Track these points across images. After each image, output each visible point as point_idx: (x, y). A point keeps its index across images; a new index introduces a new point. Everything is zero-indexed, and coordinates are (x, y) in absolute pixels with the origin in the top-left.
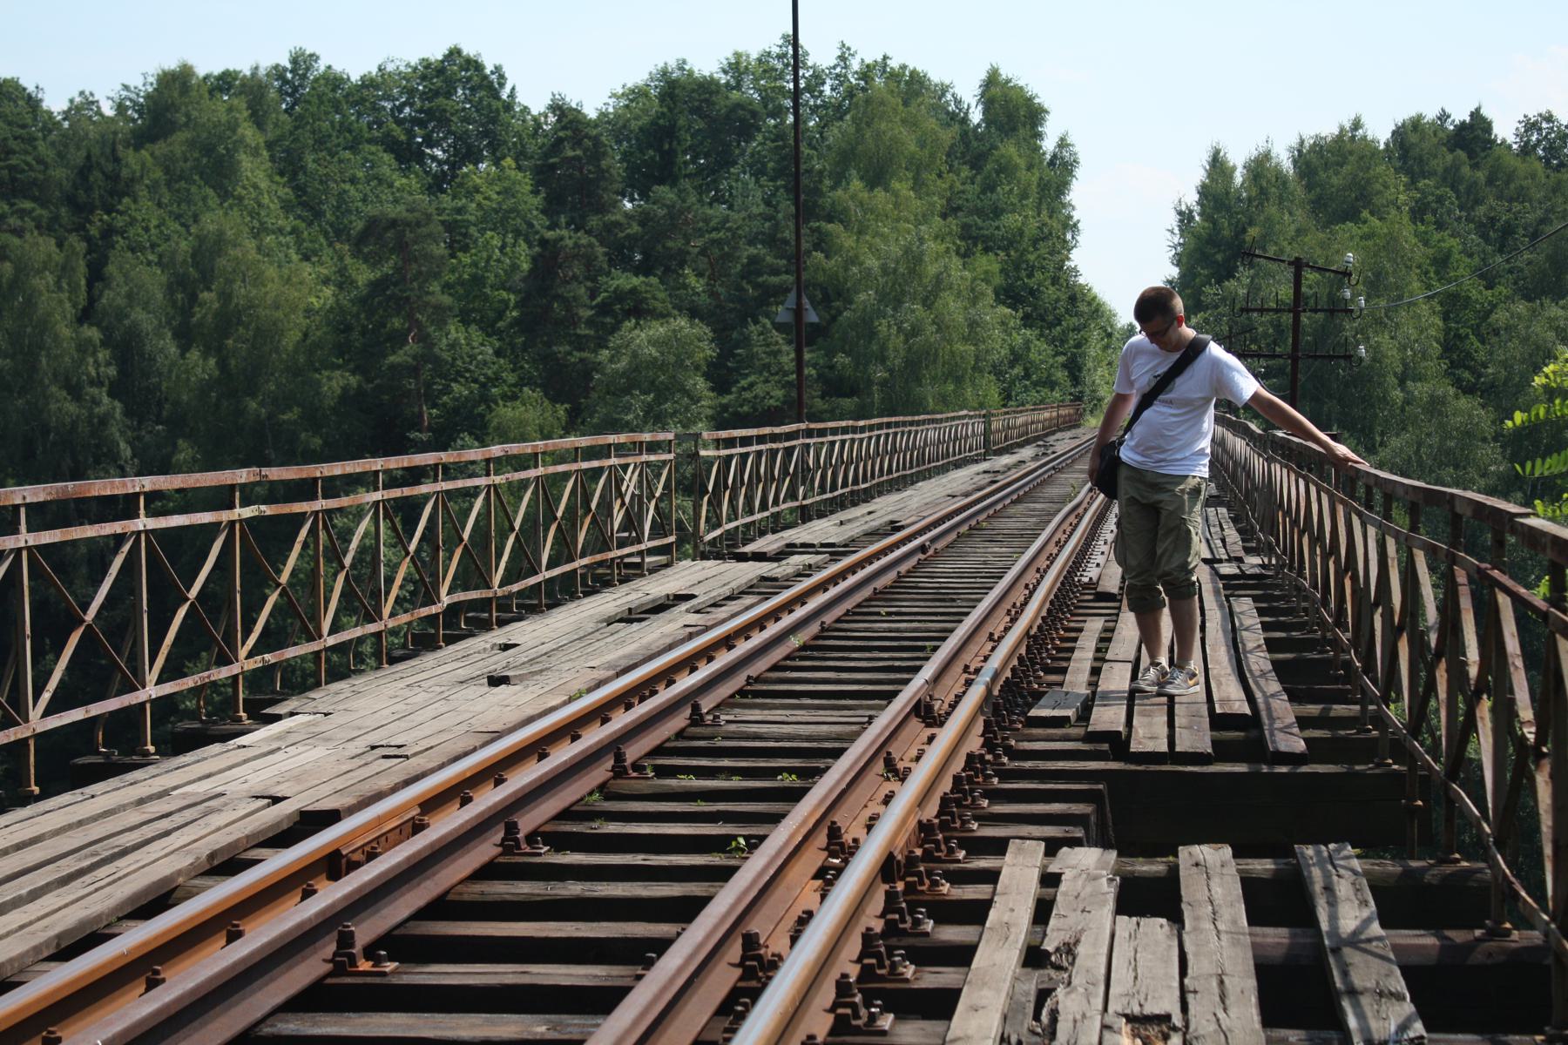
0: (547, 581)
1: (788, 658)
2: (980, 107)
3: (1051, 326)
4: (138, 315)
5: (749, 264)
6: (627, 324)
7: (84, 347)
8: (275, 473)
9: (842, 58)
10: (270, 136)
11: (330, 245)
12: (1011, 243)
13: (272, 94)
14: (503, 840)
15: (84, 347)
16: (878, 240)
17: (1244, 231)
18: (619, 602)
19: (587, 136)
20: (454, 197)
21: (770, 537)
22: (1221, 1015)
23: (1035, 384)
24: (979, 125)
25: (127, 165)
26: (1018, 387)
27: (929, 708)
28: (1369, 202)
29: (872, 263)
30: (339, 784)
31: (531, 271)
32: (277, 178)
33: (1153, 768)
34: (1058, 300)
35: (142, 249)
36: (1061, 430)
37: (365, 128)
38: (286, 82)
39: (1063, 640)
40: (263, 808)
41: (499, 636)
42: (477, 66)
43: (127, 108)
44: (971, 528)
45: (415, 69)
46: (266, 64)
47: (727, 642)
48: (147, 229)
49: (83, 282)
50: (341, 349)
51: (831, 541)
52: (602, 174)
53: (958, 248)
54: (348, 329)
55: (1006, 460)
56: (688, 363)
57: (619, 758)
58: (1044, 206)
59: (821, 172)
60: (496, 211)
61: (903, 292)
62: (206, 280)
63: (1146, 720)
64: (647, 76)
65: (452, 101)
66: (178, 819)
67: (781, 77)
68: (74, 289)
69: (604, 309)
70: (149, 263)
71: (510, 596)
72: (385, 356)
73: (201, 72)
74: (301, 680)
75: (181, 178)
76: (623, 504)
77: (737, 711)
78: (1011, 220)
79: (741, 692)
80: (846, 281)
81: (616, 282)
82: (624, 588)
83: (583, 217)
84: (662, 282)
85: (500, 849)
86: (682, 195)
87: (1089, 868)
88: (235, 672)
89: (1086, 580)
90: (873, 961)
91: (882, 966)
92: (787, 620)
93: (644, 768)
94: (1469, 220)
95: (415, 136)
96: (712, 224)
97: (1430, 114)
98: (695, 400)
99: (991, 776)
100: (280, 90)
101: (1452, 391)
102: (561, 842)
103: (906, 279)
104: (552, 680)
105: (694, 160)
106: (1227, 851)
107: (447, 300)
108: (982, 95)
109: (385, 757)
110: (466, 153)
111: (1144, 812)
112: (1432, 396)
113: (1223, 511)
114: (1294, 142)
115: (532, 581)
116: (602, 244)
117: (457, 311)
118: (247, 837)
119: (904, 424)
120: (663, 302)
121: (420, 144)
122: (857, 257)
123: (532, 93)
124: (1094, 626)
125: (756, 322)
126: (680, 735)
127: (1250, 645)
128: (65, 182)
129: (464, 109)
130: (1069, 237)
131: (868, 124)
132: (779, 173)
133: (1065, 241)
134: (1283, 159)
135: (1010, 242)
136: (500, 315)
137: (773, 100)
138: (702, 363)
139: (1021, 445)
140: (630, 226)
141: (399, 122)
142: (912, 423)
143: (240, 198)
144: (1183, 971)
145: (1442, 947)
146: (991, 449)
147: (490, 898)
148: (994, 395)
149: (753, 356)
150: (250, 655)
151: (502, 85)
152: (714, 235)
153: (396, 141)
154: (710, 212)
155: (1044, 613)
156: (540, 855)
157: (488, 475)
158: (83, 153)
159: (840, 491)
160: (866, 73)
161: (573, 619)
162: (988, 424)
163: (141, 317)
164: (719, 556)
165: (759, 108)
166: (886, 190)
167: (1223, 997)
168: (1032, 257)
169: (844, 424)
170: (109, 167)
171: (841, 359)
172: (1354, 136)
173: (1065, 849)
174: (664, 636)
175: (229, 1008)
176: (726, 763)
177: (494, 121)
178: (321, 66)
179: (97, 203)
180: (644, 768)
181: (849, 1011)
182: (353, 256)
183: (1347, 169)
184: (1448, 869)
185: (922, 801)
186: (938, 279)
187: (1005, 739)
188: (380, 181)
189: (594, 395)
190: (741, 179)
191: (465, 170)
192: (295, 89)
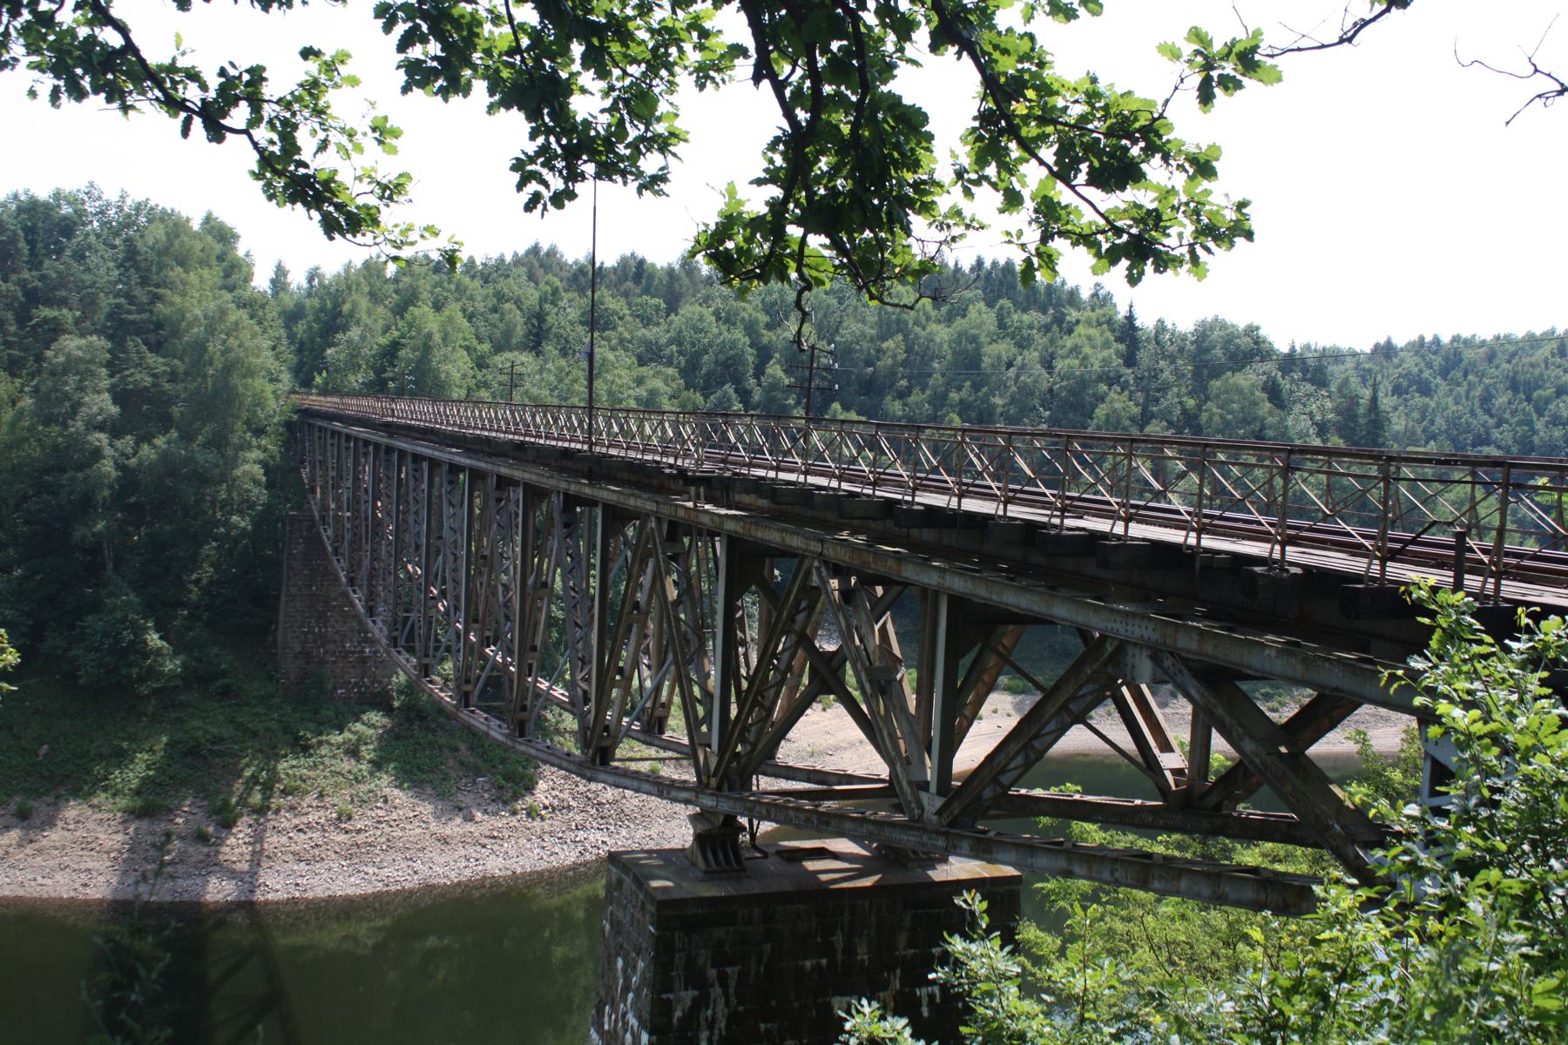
160: (138, 208)
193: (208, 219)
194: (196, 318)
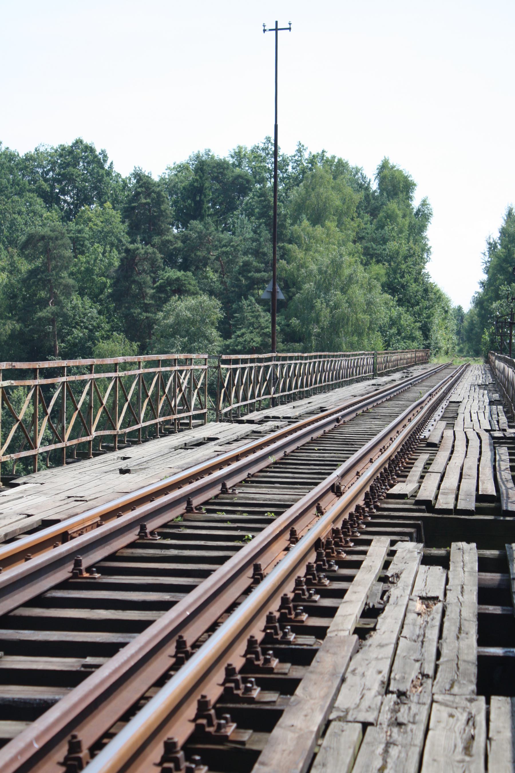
1: (268, 467)
2: (377, 181)
3: (413, 306)
5: (243, 266)
6: (174, 297)
8: (19, 365)
9: (299, 151)
11: (6, 248)
12: (392, 258)
14: (140, 533)
16: (317, 255)
18: (179, 440)
19: (153, 191)
20: (77, 224)
21: (255, 413)
22: (460, 597)
23: (404, 338)
24: (375, 191)
26: (393, 340)
27: (339, 488)
29: (313, 267)
30: (58, 510)
31: (120, 267)
33: (445, 516)
34: (417, 291)
36: (416, 364)
37: (27, 183)
39: (407, 463)
40: (24, 518)
42: (92, 150)
44: (363, 412)
45: (56, 151)
47: (237, 458)
50: (11, 308)
52: (162, 213)
55: (385, 379)
56: (207, 320)
57: (189, 503)
58: (411, 238)
59: (285, 215)
61: (330, 284)
63: (444, 496)
64: (188, 158)
67: (264, 160)
69: (161, 289)
72: (35, 313)
76: (180, 390)
77: (243, 488)
78: (392, 245)
79: (245, 481)
80: (298, 277)
81: (167, 275)
82: (181, 434)
83: (150, 237)
84: (194, 275)
85: (138, 537)
86: (206, 226)
87: (410, 550)
89: (422, 437)
90: (311, 577)
91: (315, 579)
92: (266, 450)
96: (223, 243)
98: (211, 342)
102: (165, 536)
103: (330, 279)
104: (150, 472)
106: (474, 545)
107: (71, 281)
109: (76, 501)
110: (84, 199)
111: (436, 531)
113: (500, 407)
115: (136, 427)
116: (160, 252)
117: (77, 288)
118: (20, 529)
119: (329, 356)
120: (194, 286)
121: (58, 193)
122: (305, 263)
123: (123, 165)
124: (424, 457)
125: (246, 299)
126: (216, 497)
127: (503, 468)
129: (83, 174)
130: (425, 256)
131: (313, 189)
132: (262, 215)
133: (422, 258)
136: (101, 292)
137: (260, 174)
139: (394, 372)
140: (176, 242)
141: (46, 180)
142: (333, 356)
146: (376, 373)
148: (380, 343)
149: (244, 318)
151: (105, 161)
152: (224, 249)
153: (44, 192)
154: (222, 236)
155: (399, 450)
156: (156, 540)
157: (116, 371)
159: (293, 391)
160: (312, 161)
161: (157, 447)
164: (229, 421)
166: (323, 227)
167: (462, 592)
168: (403, 266)
169: (296, 354)
171: (294, 321)
173: (399, 542)
174: (204, 455)
175: (33, 585)
177: (100, 181)
180: (201, 508)
181: (300, 592)
182: (19, 255)
185: (335, 520)
186: (350, 278)
188: (35, 213)
189: (154, 338)
190: (239, 218)
191: (83, 208)
193: (384, 166)
194: (310, 273)
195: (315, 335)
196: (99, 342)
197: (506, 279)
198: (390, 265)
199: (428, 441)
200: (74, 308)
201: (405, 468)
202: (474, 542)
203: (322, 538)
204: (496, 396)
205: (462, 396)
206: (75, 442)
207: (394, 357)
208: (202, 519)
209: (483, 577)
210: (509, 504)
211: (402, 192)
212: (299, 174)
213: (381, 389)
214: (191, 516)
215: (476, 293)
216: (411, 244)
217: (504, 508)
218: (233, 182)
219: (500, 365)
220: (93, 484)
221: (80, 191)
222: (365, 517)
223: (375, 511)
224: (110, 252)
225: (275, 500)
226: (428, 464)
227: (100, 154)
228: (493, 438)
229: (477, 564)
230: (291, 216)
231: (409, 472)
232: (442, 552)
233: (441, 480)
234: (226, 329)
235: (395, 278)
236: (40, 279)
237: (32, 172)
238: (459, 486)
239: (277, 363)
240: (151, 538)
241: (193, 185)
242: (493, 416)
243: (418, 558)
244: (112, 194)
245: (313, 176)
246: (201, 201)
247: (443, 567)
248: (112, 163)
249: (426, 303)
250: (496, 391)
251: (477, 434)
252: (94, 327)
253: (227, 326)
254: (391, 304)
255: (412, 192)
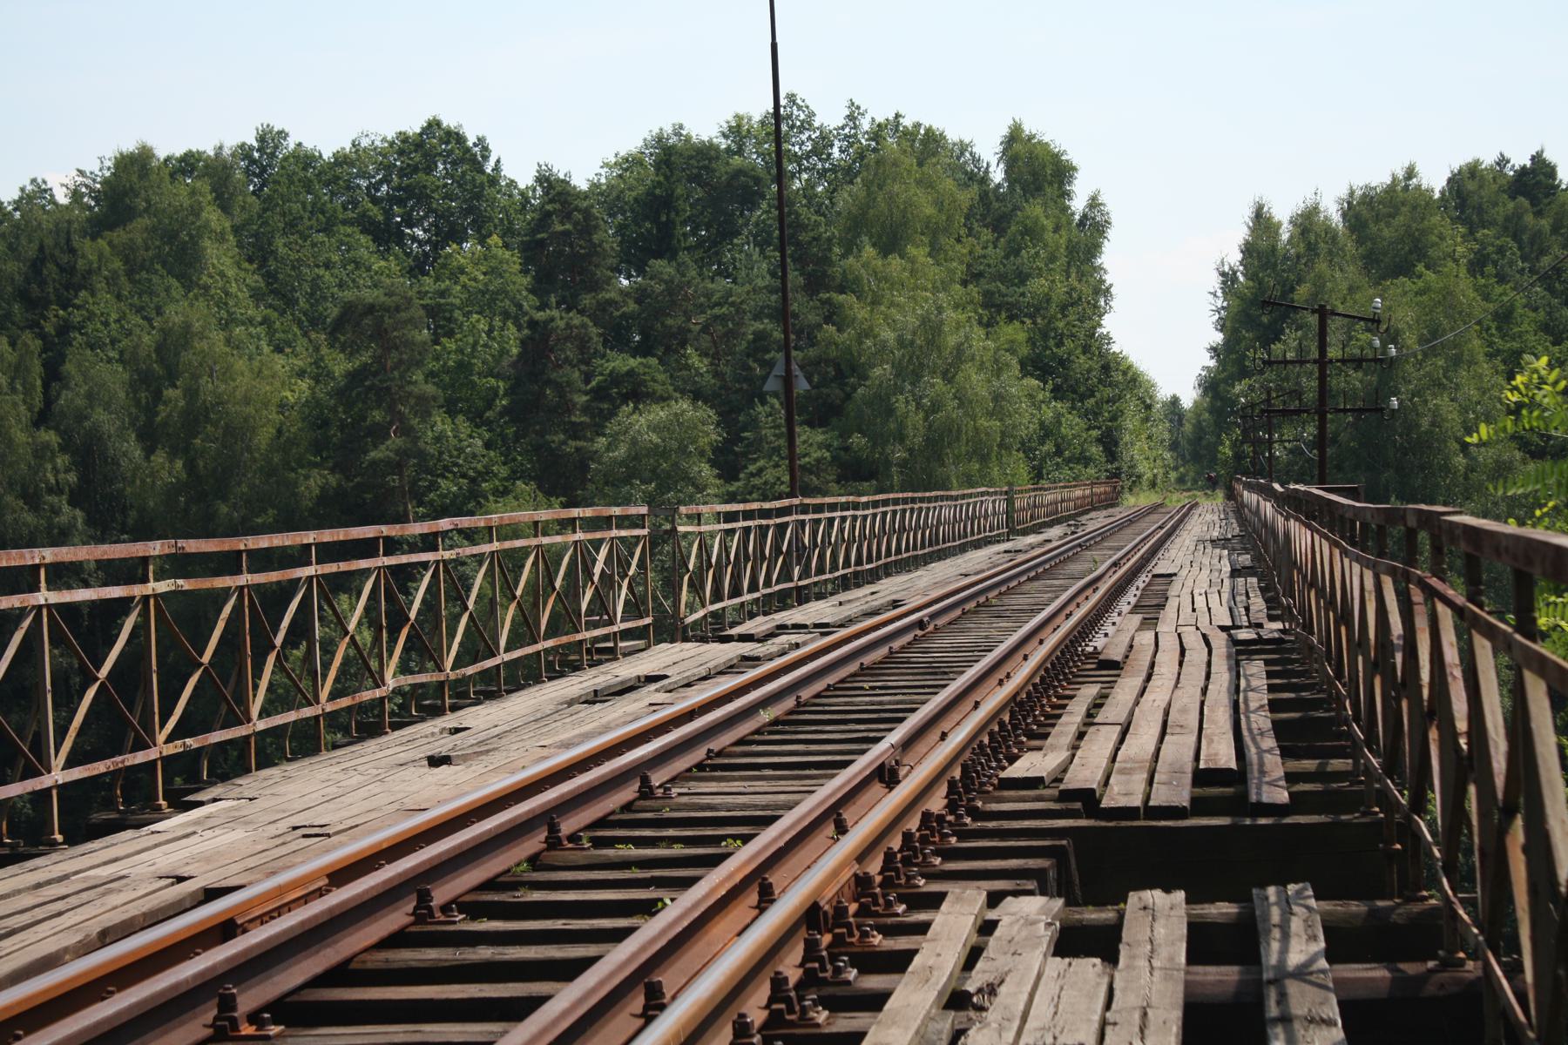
0: (507, 664)
2: (1002, 166)
3: (1082, 398)
4: (100, 416)
5: (754, 341)
6: (625, 408)
7: (41, 452)
8: (193, 546)
9: (851, 117)
10: (238, 221)
11: (305, 334)
12: (1038, 310)
13: (238, 175)
15: (41, 452)
16: (893, 310)
17: (1292, 289)
18: (585, 685)
19: (577, 209)
20: (437, 279)
21: (760, 619)
23: (1068, 461)
24: (999, 186)
25: (83, 256)
28: (1425, 256)
29: (888, 335)
30: (251, 862)
31: (520, 355)
32: (246, 265)
33: (1124, 824)
34: (1089, 371)
35: (102, 347)
36: (1094, 509)
37: (340, 209)
38: (253, 161)
41: (450, 721)
43: (83, 195)
45: (392, 144)
46: (231, 142)
48: (106, 324)
49: (39, 382)
50: (318, 447)
51: (825, 621)
52: (595, 250)
53: (981, 316)
54: (326, 424)
55: (1032, 539)
56: (691, 448)
57: (553, 829)
58: (1073, 270)
59: (829, 240)
60: (483, 293)
62: (172, 377)
63: (1123, 777)
65: (431, 177)
66: (73, 901)
68: (28, 391)
69: (599, 394)
70: (109, 361)
71: (464, 680)
72: (366, 452)
73: (161, 153)
74: (231, 764)
75: (142, 267)
77: (692, 783)
78: (1038, 285)
79: (700, 766)
80: (860, 355)
82: (594, 671)
87: (1032, 915)
88: (153, 757)
89: (1090, 649)
90: (783, 1006)
91: (791, 1010)
93: (580, 838)
94: (1532, 271)
95: (394, 216)
97: (1488, 159)
99: (948, 835)
100: (247, 171)
101: (1518, 455)
102: (475, 910)
103: (922, 355)
104: (497, 759)
105: (694, 232)
106: (1180, 896)
107: (430, 389)
108: (1004, 152)
109: (305, 836)
111: (1095, 863)
112: (1497, 461)
114: (1343, 193)
115: (489, 663)
117: (441, 401)
118: (144, 914)
122: (871, 329)
123: (518, 167)
124: (1089, 692)
126: (627, 807)
127: (1253, 705)
128: (17, 277)
131: (880, 187)
133: (1096, 306)
134: (1332, 211)
135: (1038, 308)
136: (490, 405)
138: (707, 448)
139: (1050, 524)
141: (375, 201)
143: (206, 288)
144: (1108, 1005)
145: (1393, 980)
146: (1013, 531)
147: (395, 966)
148: (1023, 471)
149: (760, 440)
150: (169, 740)
151: (486, 158)
152: (717, 311)
153: (372, 222)
154: (710, 286)
156: (454, 923)
158: (35, 246)
160: (878, 133)
162: (1010, 502)
163: (102, 418)
164: (703, 640)
165: (762, 174)
166: (902, 257)
168: (1061, 324)
170: (64, 259)
171: (857, 440)
172: (1407, 186)
173: (1009, 898)
176: (671, 832)
177: (478, 196)
178: (291, 144)
179: (52, 297)
180: (580, 838)
182: (332, 346)
183: (1400, 220)
184: (1416, 908)
185: (862, 856)
186: (959, 349)
187: (970, 800)
188: (357, 264)
189: (591, 487)
190: (743, 249)
192: (263, 169)
194: (883, 347)
195: (897, 465)
196: (487, 499)
197: (1258, 339)
198: (1034, 323)
199: (1101, 657)
200: (438, 439)
201: (1048, 717)
202: (1179, 888)
203: (822, 904)
204: (1245, 559)
205: (1178, 563)
206: (344, 702)
207: (1049, 497)
208: (582, 862)
209: (1198, 978)
210: (1265, 788)
211: (1051, 184)
212: (854, 162)
213: (1021, 558)
214: (557, 856)
215: (1204, 368)
216: (1073, 280)
217: (1253, 798)
218: (729, 184)
219: (1250, 497)
220: (363, 793)
221: (442, 217)
222: (944, 836)
223: (968, 820)
224: (502, 329)
225: (755, 807)
226: (1097, 705)
227: (475, 145)
228: (1235, 642)
229: (1184, 945)
230: (841, 239)
231: (1053, 725)
232: (1106, 915)
233: (1121, 741)
234: (728, 463)
235: (1047, 348)
236: (370, 388)
237: (348, 188)
238: (1158, 750)
239: (802, 517)
240: (443, 918)
241: (653, 194)
242: (1238, 599)
243: (1045, 936)
244: (501, 220)
245: (878, 162)
246: (670, 225)
247: (1103, 960)
248: (498, 161)
249: (1109, 392)
250: (1247, 551)
251: (1204, 636)
252: (479, 473)
253: (731, 457)
254: (1041, 397)
255: (1070, 183)
